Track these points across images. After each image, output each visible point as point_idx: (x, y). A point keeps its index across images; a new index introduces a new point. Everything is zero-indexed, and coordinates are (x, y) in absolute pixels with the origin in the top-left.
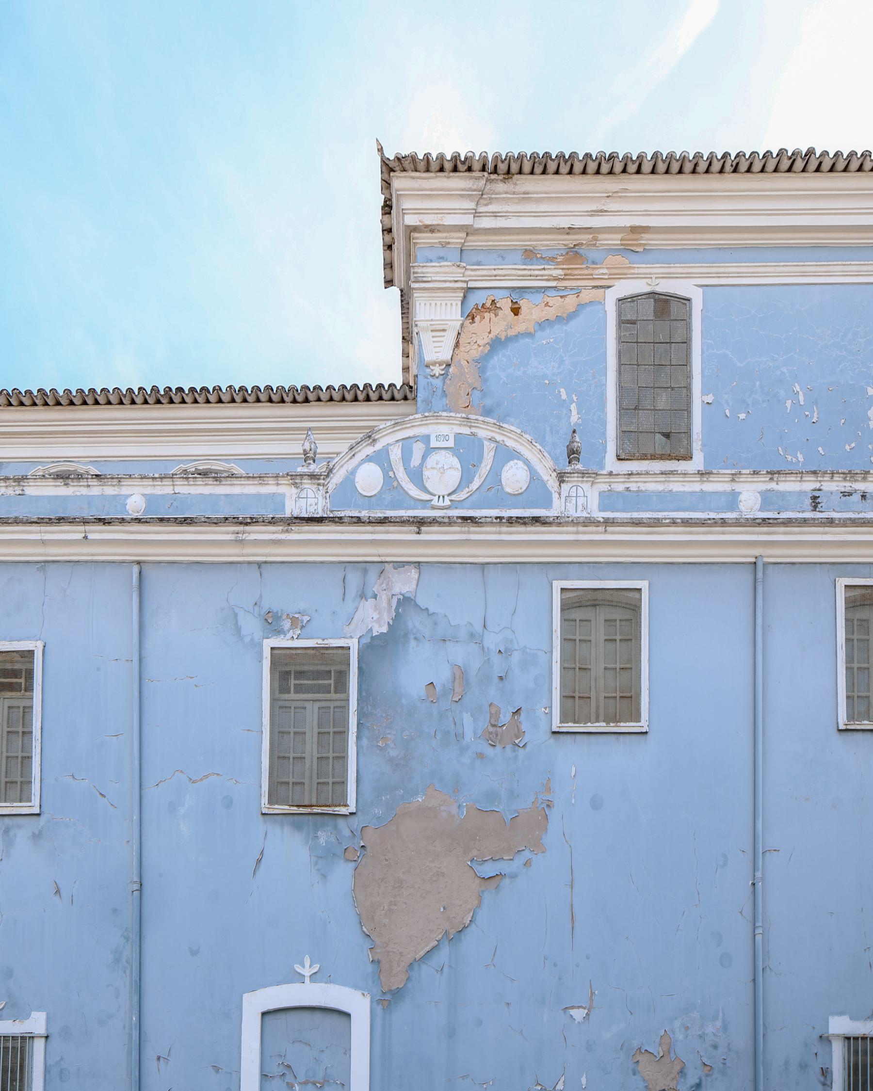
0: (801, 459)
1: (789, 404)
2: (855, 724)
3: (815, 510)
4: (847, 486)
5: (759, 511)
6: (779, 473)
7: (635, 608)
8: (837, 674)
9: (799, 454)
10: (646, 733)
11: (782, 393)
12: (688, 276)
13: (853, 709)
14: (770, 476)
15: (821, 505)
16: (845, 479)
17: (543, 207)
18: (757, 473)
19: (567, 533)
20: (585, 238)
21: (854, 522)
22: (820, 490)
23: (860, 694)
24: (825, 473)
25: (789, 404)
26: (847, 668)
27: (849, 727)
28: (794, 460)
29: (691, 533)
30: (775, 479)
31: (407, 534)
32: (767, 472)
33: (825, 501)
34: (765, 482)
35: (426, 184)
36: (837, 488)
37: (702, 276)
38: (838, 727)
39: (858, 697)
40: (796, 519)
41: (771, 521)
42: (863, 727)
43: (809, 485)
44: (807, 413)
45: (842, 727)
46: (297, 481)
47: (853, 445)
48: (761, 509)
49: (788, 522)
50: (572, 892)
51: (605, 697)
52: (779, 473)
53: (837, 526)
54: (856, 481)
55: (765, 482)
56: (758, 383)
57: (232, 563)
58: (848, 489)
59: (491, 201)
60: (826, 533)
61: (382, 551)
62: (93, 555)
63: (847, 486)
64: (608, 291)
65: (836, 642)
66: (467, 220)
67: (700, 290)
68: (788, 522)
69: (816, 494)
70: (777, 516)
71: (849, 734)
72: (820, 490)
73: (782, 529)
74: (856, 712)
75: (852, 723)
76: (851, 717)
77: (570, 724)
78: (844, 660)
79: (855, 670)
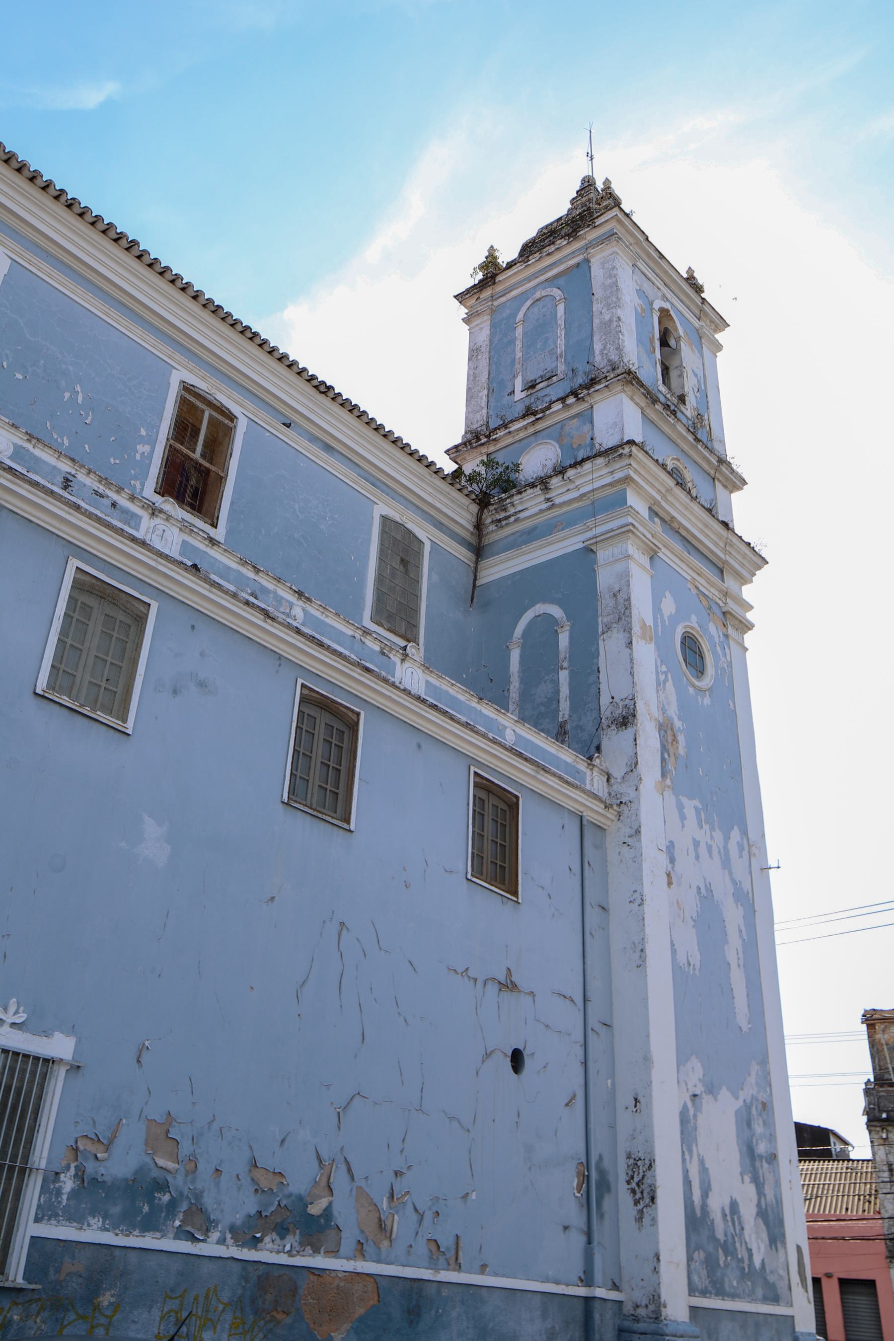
0: (66, 442)
1: (67, 395)
2: (53, 695)
3: (65, 490)
4: (101, 489)
5: (8, 458)
6: (38, 440)
7: (141, 620)
8: (47, 640)
9: (65, 438)
10: (129, 735)
11: (63, 383)
12: (242, 406)
13: (56, 680)
14: (28, 437)
15: (72, 489)
16: (100, 482)
18: (16, 428)
19: (555, 782)
21: (99, 520)
22: (74, 476)
23: (66, 669)
24: (84, 466)
25: (67, 395)
26: (59, 639)
27: (46, 695)
28: (59, 440)
30: (33, 443)
31: (258, 619)
32: (27, 432)
33: (76, 487)
34: (22, 439)
35: (383, 444)
36: (91, 485)
37: (12, 251)
38: (35, 689)
39: (64, 671)
40: (44, 486)
41: (17, 473)
42: (61, 701)
43: (65, 467)
44: (82, 413)
45: (39, 691)
46: (356, 635)
47: (118, 462)
48: (10, 458)
49: (35, 484)
51: (90, 682)
52: (38, 440)
53: (82, 514)
54: (110, 489)
55: (22, 439)
56: (42, 362)
57: (250, 638)
58: (100, 491)
60: (69, 514)
61: (447, 736)
63: (101, 489)
64: (375, 505)
65: (55, 610)
67: (10, 261)
68: (35, 484)
69: (71, 478)
70: (26, 473)
71: (46, 701)
72: (74, 476)
73: (27, 486)
74: (58, 684)
75: (51, 692)
76: (51, 685)
77: (65, 698)
78: (58, 631)
79: (68, 645)
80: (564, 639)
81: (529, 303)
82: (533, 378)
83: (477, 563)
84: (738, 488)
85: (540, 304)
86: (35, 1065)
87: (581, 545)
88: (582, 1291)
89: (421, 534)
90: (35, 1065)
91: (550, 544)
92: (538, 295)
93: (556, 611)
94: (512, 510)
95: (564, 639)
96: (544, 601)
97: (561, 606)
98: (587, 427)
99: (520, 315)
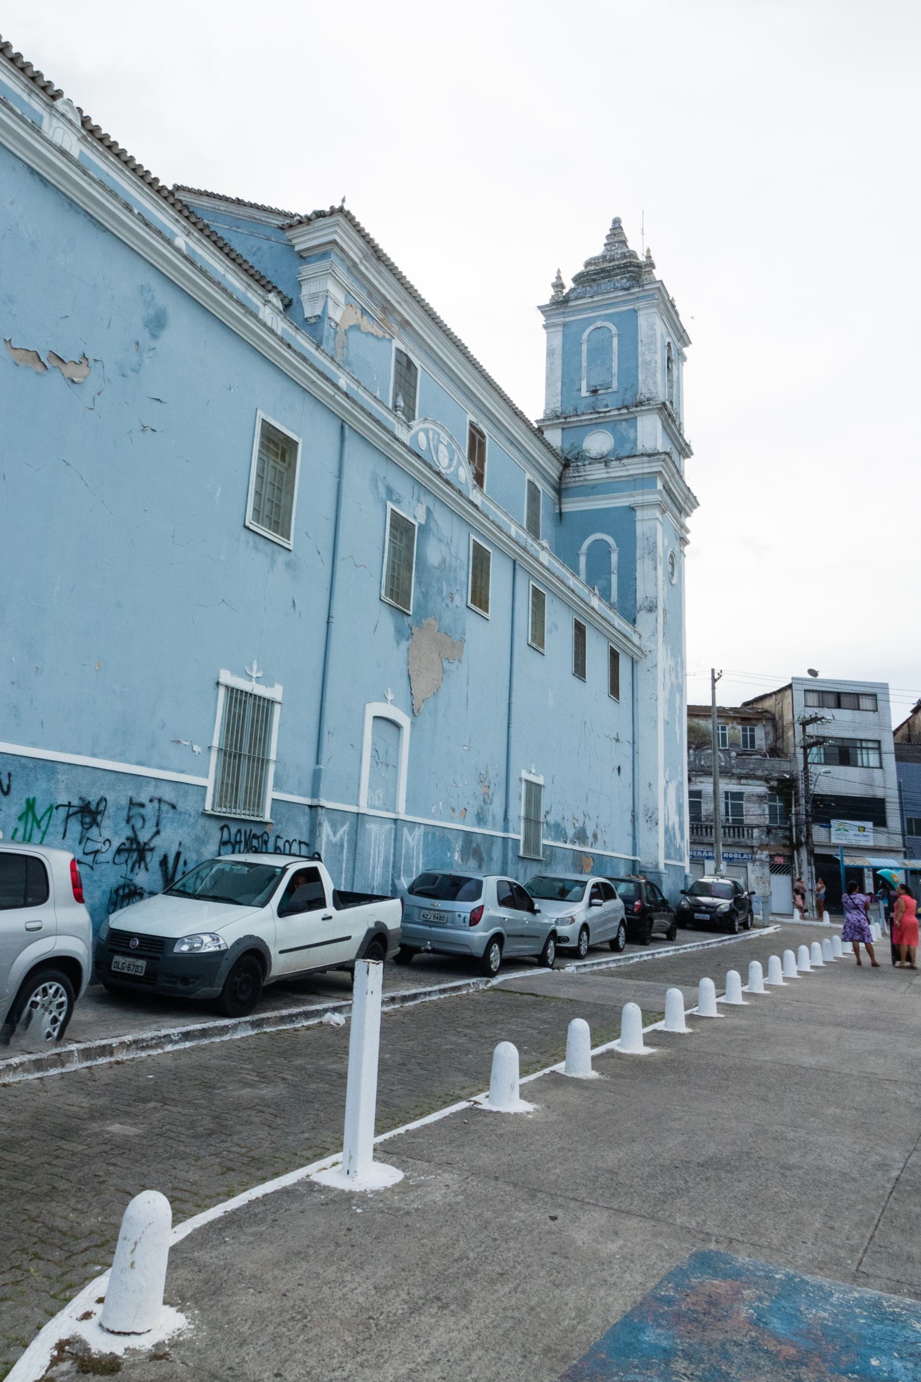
17: (382, 281)
20: (390, 308)
29: (174, 255)
50: (782, 962)
59: (367, 261)
62: (59, 183)
66: (357, 261)
80: (614, 557)
81: (592, 328)
82: (595, 384)
83: (560, 499)
84: (688, 457)
85: (600, 331)
86: (241, 694)
87: (627, 504)
88: (632, 858)
89: (540, 487)
90: (241, 694)
91: (606, 499)
92: (599, 324)
93: (610, 540)
94: (583, 474)
95: (614, 557)
96: (602, 532)
97: (613, 537)
98: (632, 431)
99: (585, 336)
